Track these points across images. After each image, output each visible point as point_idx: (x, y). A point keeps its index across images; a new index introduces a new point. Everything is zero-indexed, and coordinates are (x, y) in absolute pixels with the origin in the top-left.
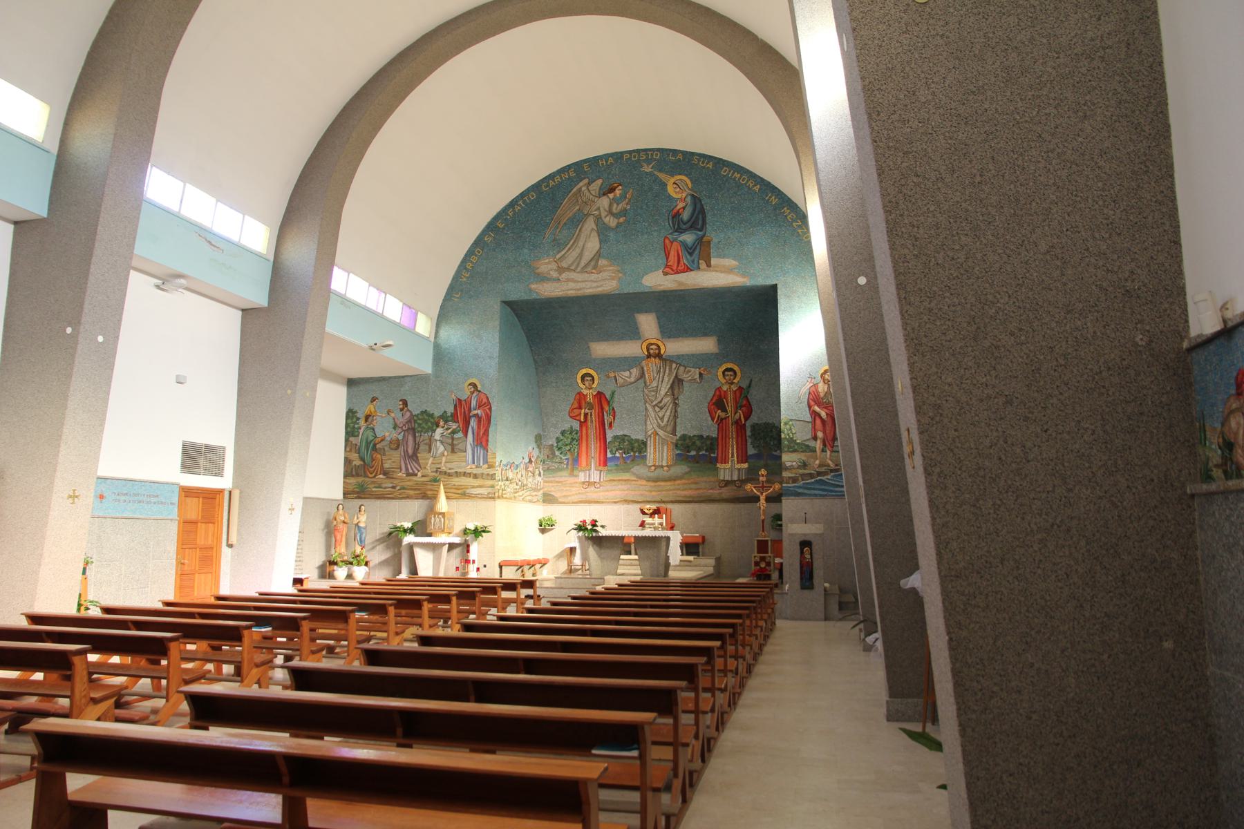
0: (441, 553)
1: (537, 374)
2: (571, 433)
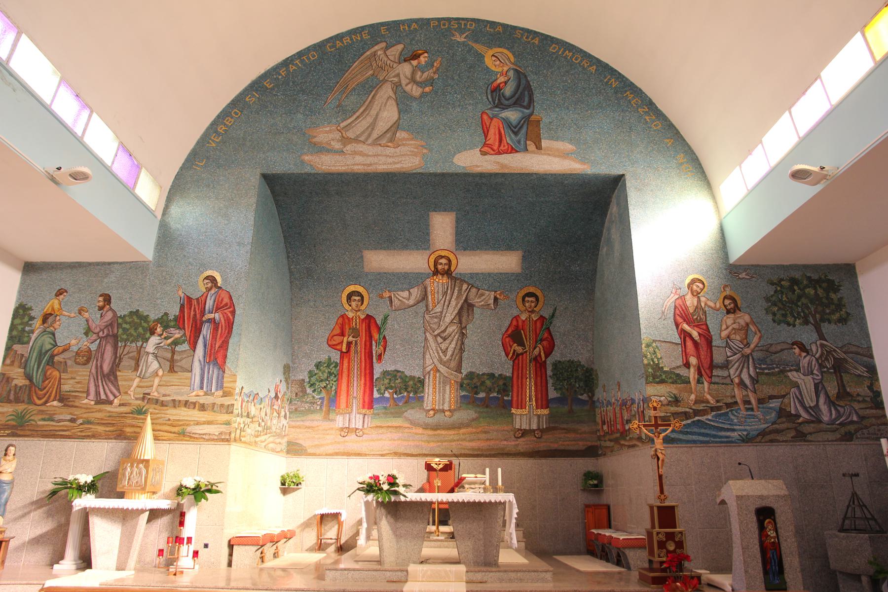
0: (134, 527)
1: (291, 289)
2: (328, 366)
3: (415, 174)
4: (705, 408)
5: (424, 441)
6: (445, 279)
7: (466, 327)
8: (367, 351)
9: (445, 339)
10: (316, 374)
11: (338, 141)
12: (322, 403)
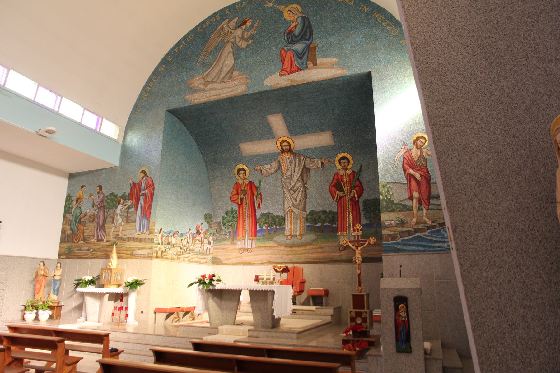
2: (232, 213)
3: (243, 95)
4: (424, 227)
5: (285, 254)
6: (289, 155)
7: (306, 183)
8: (252, 203)
9: (295, 191)
10: (226, 218)
11: (203, 84)
12: (230, 234)
